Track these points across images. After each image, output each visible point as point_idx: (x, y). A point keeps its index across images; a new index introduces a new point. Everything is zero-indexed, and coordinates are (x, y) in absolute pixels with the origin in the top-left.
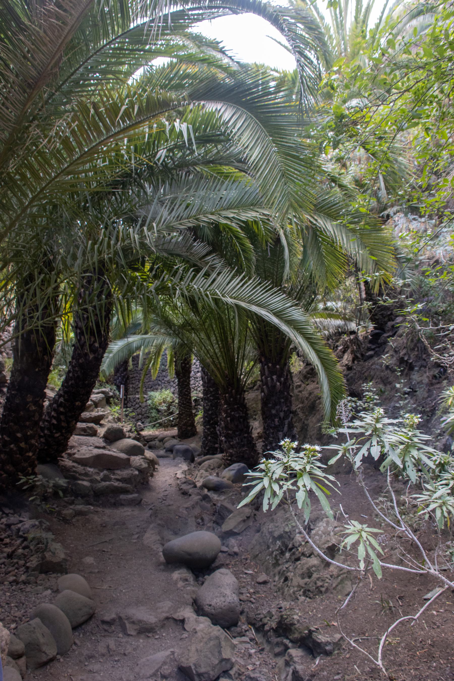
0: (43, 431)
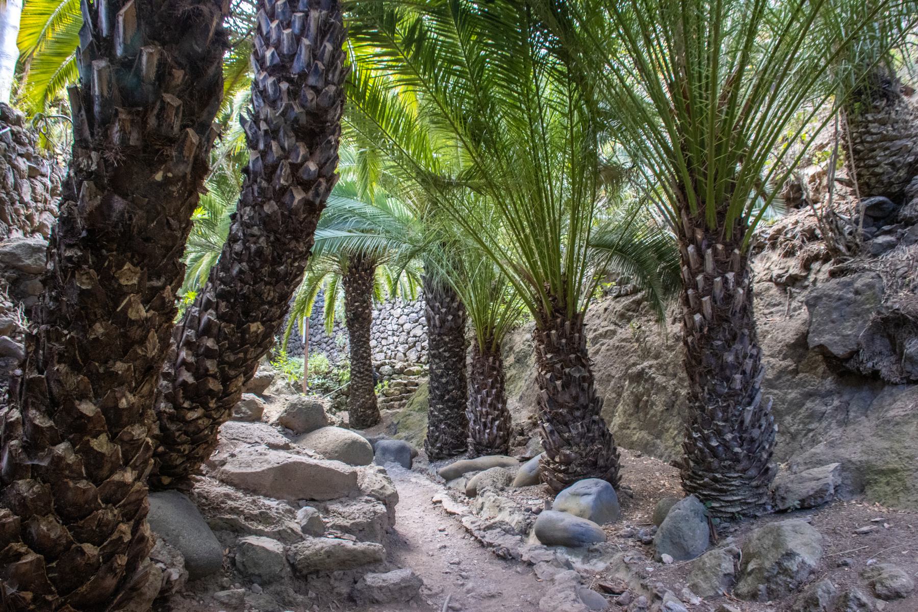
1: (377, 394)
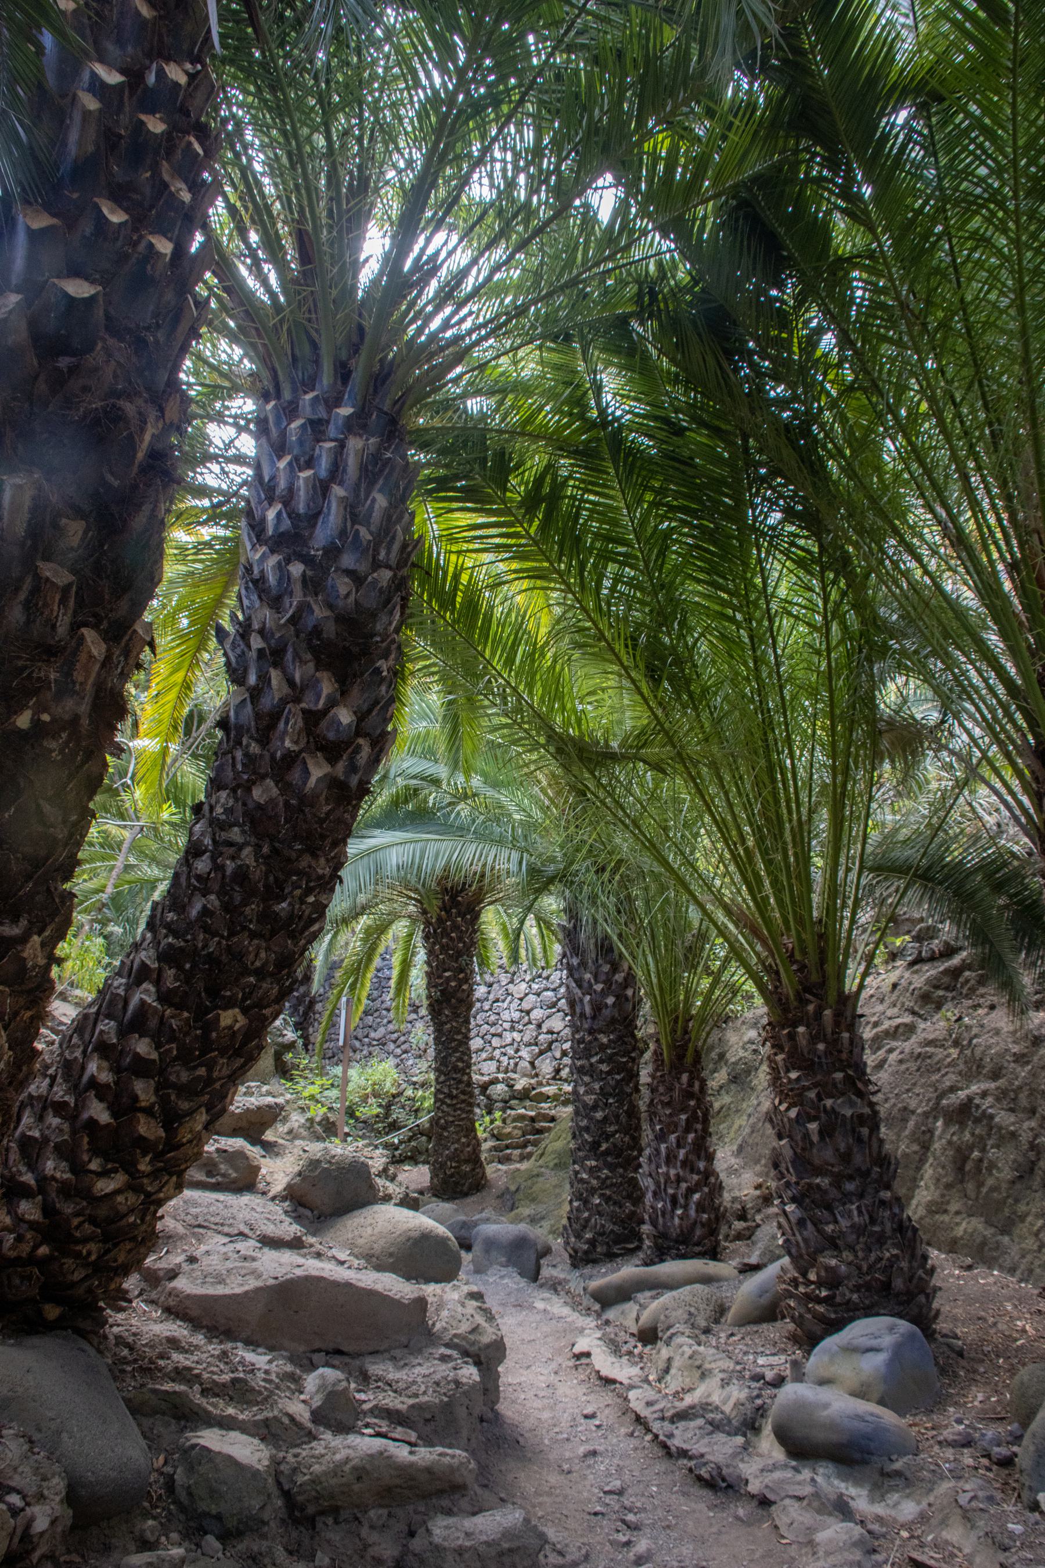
0: (32, 1160)
1: (481, 1134)
